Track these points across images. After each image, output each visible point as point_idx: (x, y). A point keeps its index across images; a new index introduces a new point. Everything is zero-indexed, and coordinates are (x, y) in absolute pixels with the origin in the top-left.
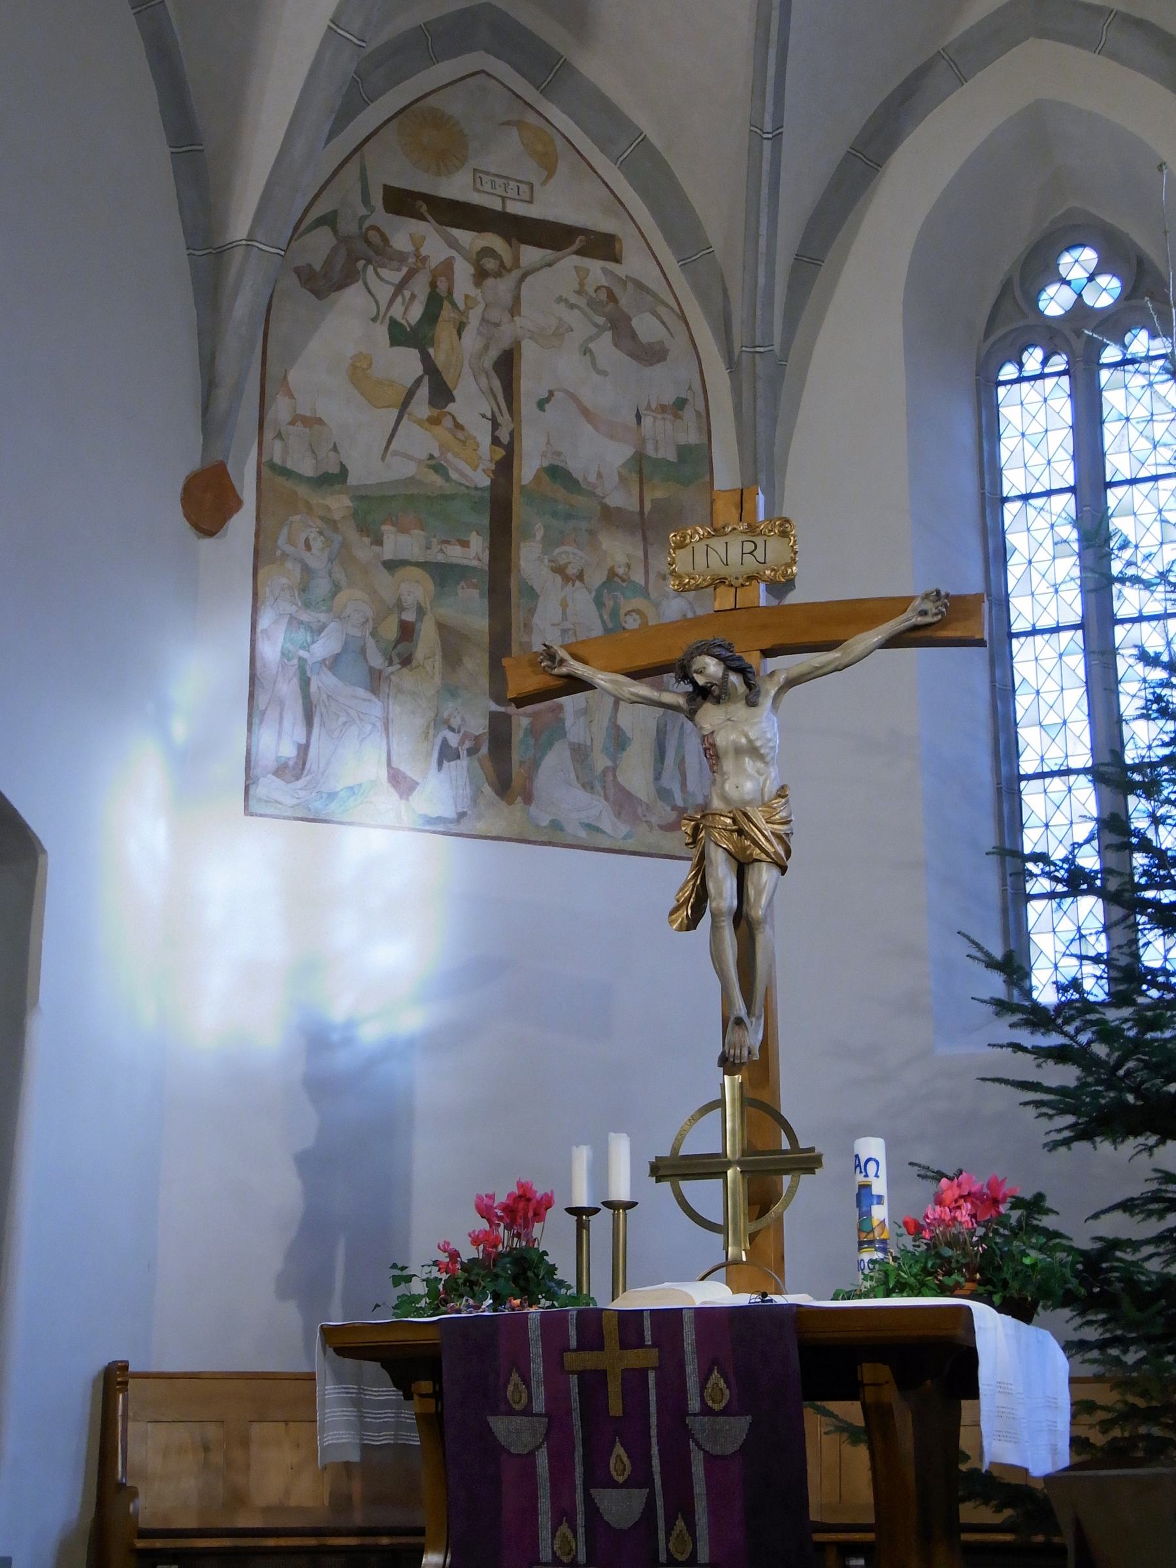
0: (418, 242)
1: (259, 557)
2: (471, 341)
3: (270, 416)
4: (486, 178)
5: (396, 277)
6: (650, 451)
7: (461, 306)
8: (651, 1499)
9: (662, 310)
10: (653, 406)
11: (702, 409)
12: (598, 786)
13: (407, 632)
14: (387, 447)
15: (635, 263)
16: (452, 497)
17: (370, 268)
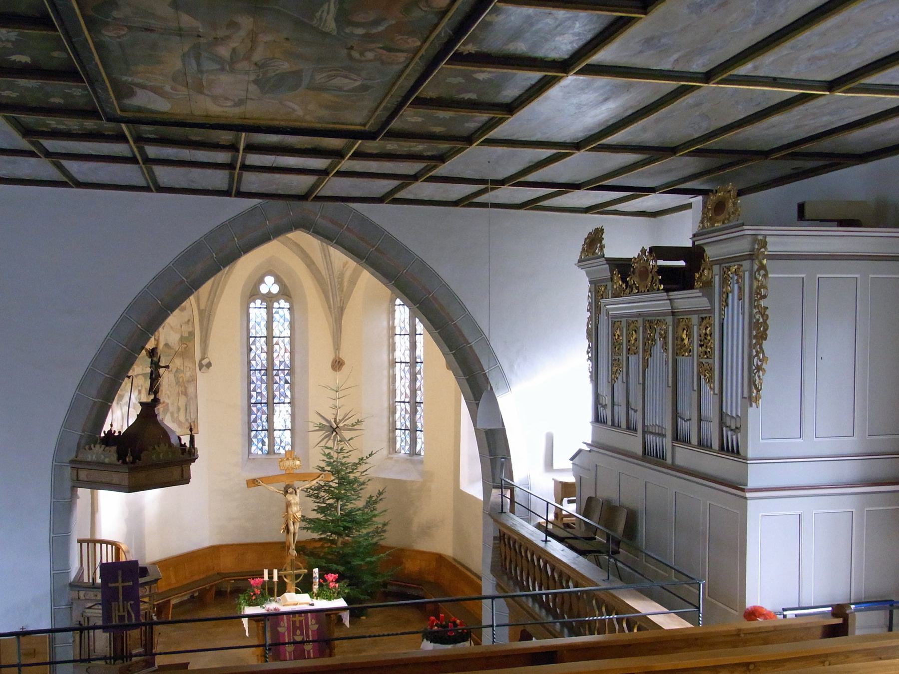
6: (184, 335)
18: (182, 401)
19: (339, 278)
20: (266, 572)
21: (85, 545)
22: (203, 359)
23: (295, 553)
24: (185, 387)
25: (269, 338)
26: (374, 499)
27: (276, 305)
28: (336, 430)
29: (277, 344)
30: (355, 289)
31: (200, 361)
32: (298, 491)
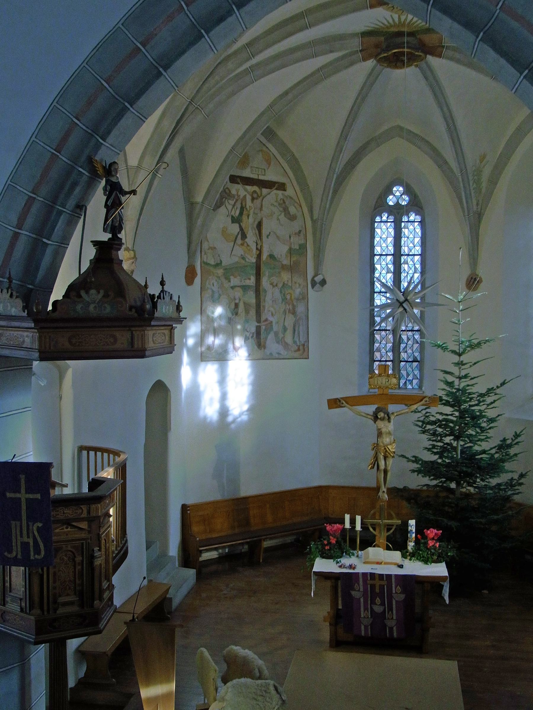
0: (238, 191)
1: (202, 289)
2: (251, 220)
3: (203, 248)
4: (254, 169)
5: (232, 202)
6: (293, 247)
7: (248, 209)
8: (385, 608)
9: (296, 204)
10: (294, 233)
11: (305, 234)
12: (280, 343)
13: (237, 305)
14: (231, 254)
15: (290, 191)
16: (247, 266)
17: (226, 200)
18: (290, 321)
19: (474, 176)
20: (347, 517)
21: (85, 453)
22: (316, 275)
23: (386, 496)
24: (293, 305)
25: (397, 255)
26: (509, 442)
27: (405, 219)
28: (404, 305)
29: (406, 263)
30: (495, 190)
31: (314, 277)
32: (392, 417)
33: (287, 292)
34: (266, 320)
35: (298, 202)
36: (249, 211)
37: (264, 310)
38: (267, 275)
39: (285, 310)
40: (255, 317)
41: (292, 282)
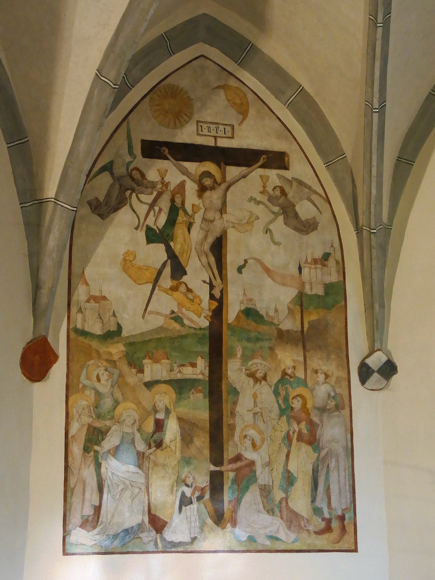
3: (74, 298)
4: (205, 126)
5: (148, 198)
6: (307, 290)
7: (190, 211)
9: (314, 197)
10: (309, 260)
14: (146, 309)
17: (134, 195)
33: (293, 393)
34: (238, 458)
35: (321, 192)
36: (192, 217)
37: (233, 436)
38: (239, 356)
39: (288, 434)
40: (207, 452)
41: (306, 370)
